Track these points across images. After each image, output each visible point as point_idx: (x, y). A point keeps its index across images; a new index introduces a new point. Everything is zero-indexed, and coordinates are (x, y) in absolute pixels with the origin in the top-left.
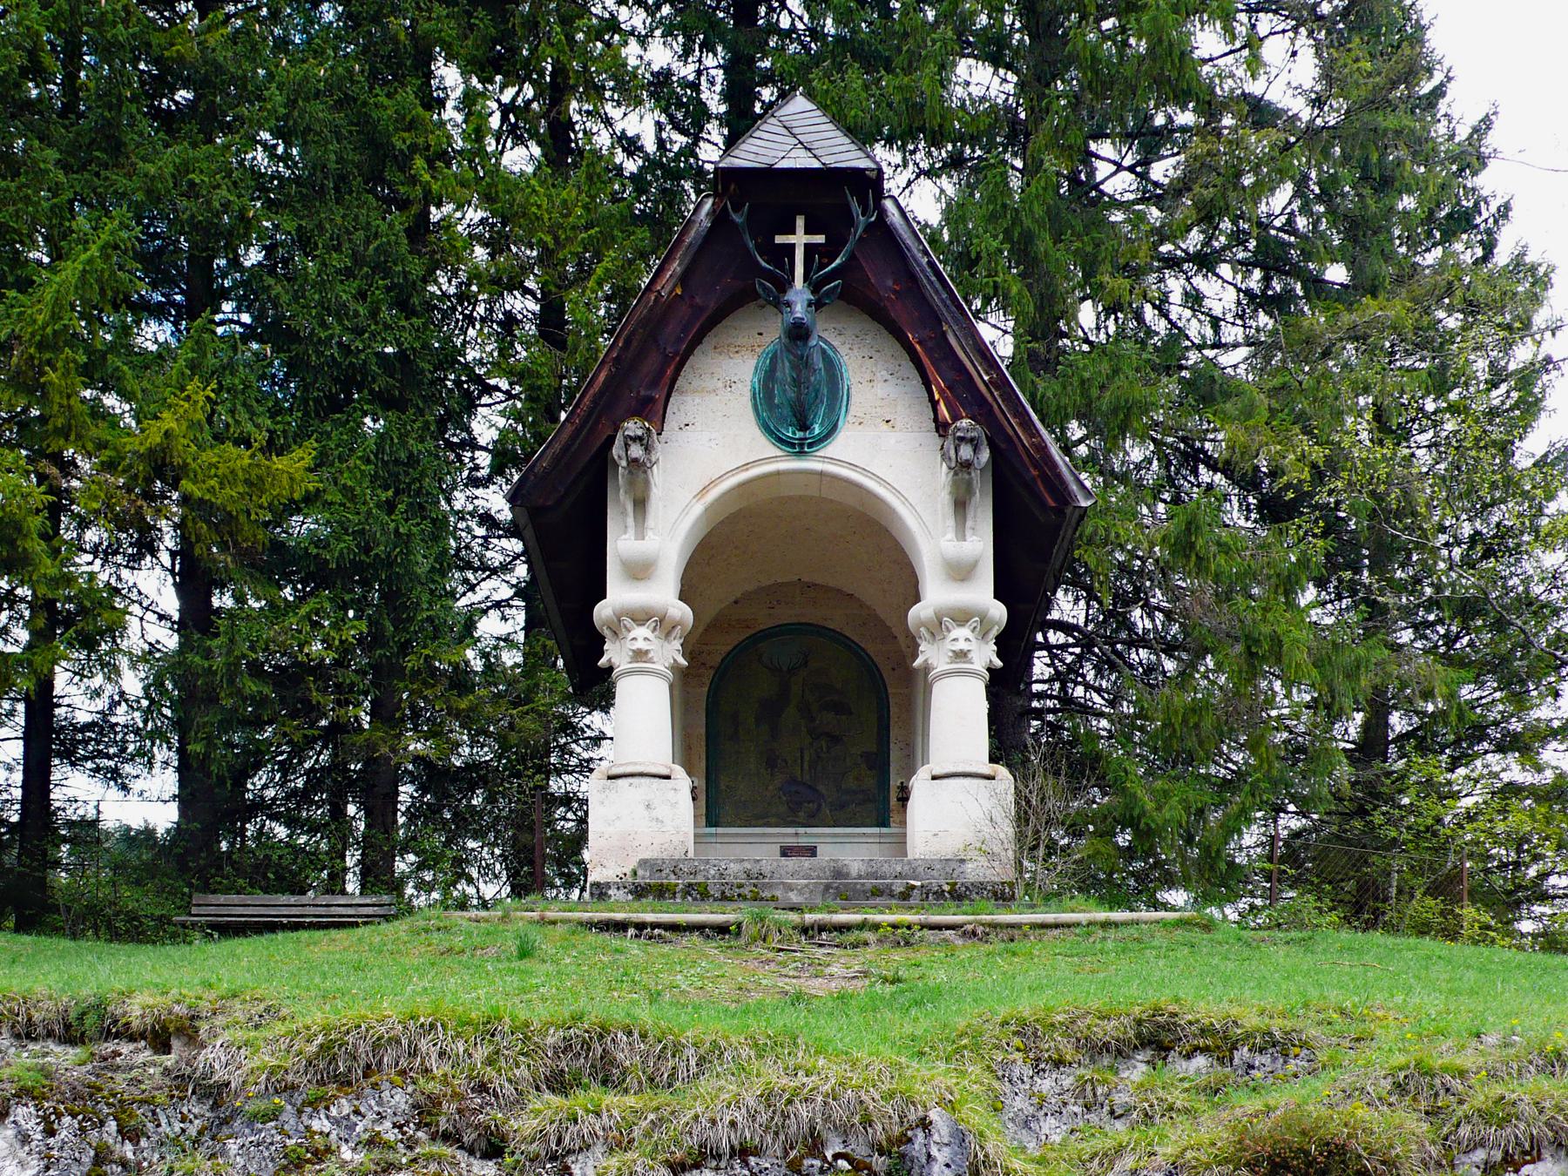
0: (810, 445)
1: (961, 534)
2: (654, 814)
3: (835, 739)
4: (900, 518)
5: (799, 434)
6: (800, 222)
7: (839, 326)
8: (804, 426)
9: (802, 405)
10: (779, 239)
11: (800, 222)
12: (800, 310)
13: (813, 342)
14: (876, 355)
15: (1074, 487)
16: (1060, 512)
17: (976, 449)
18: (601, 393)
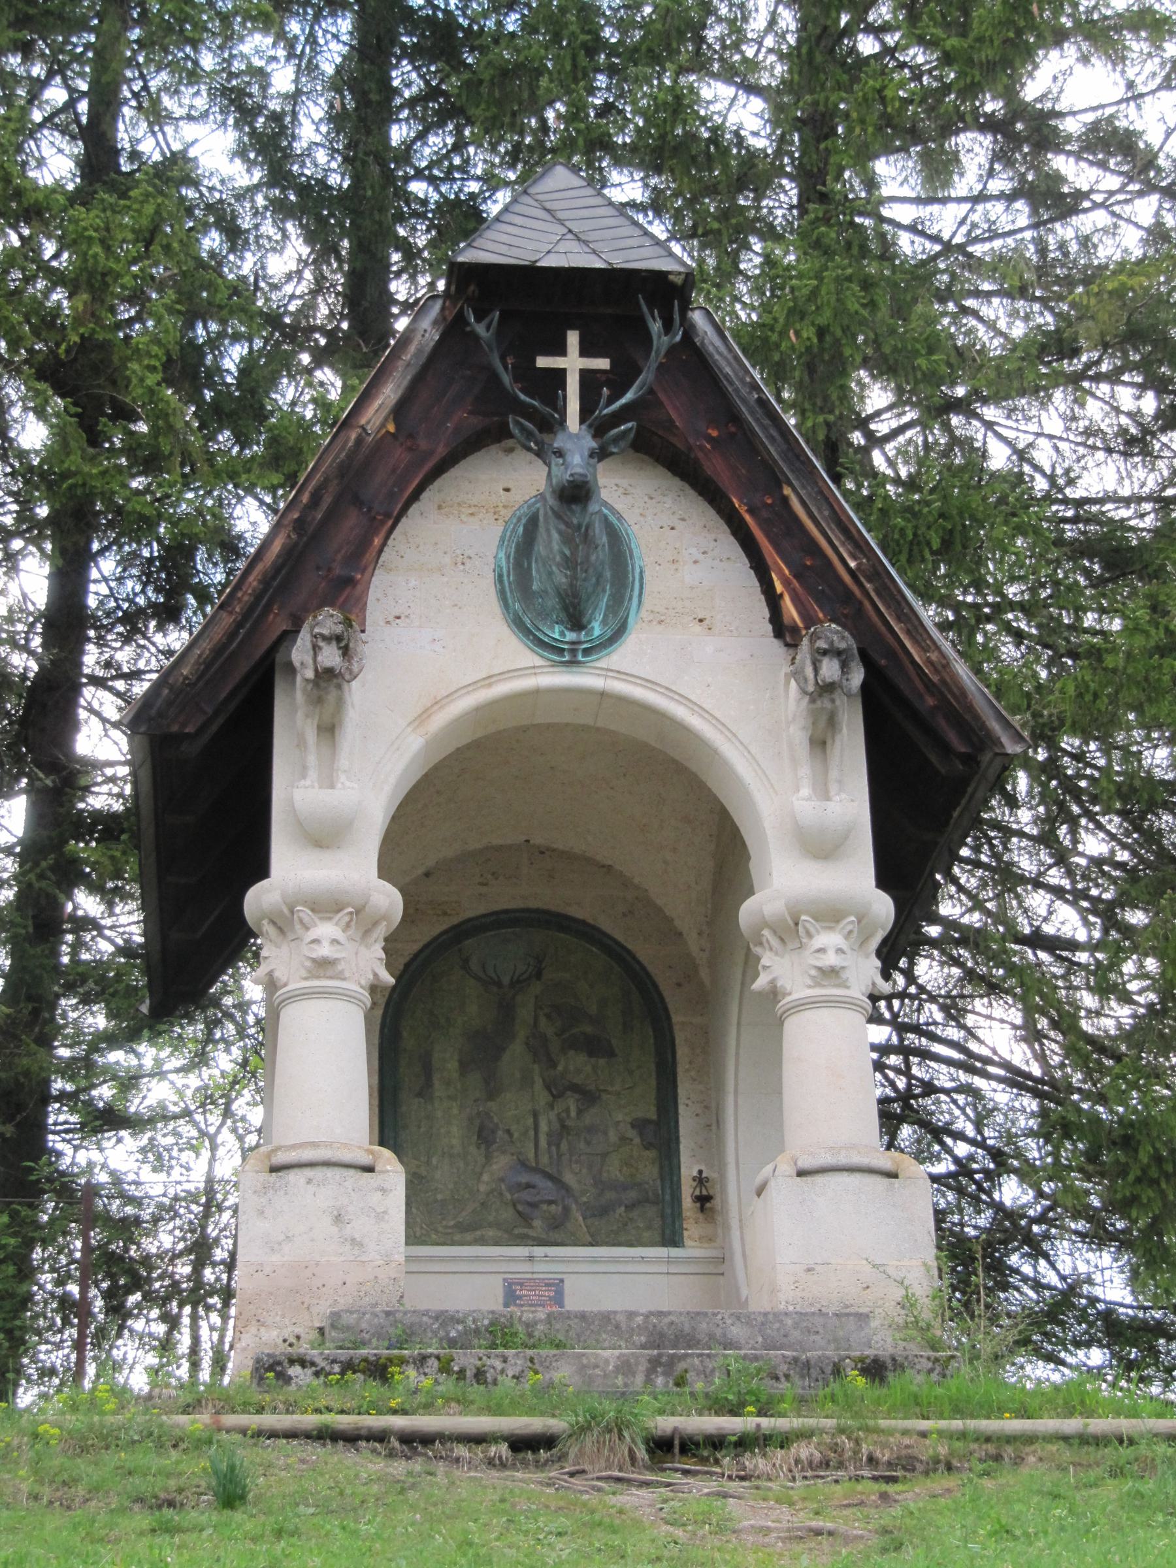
0: (587, 652)
1: (824, 793)
2: (348, 1231)
3: (589, 1097)
4: (725, 763)
5: (571, 636)
6: (573, 339)
7: (624, 483)
8: (577, 622)
9: (576, 595)
10: (542, 362)
11: (573, 339)
12: (577, 461)
13: (593, 507)
14: (680, 525)
15: (995, 726)
16: (971, 760)
17: (845, 666)
18: (277, 568)
